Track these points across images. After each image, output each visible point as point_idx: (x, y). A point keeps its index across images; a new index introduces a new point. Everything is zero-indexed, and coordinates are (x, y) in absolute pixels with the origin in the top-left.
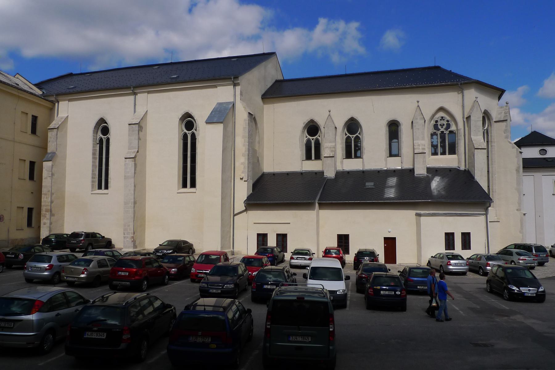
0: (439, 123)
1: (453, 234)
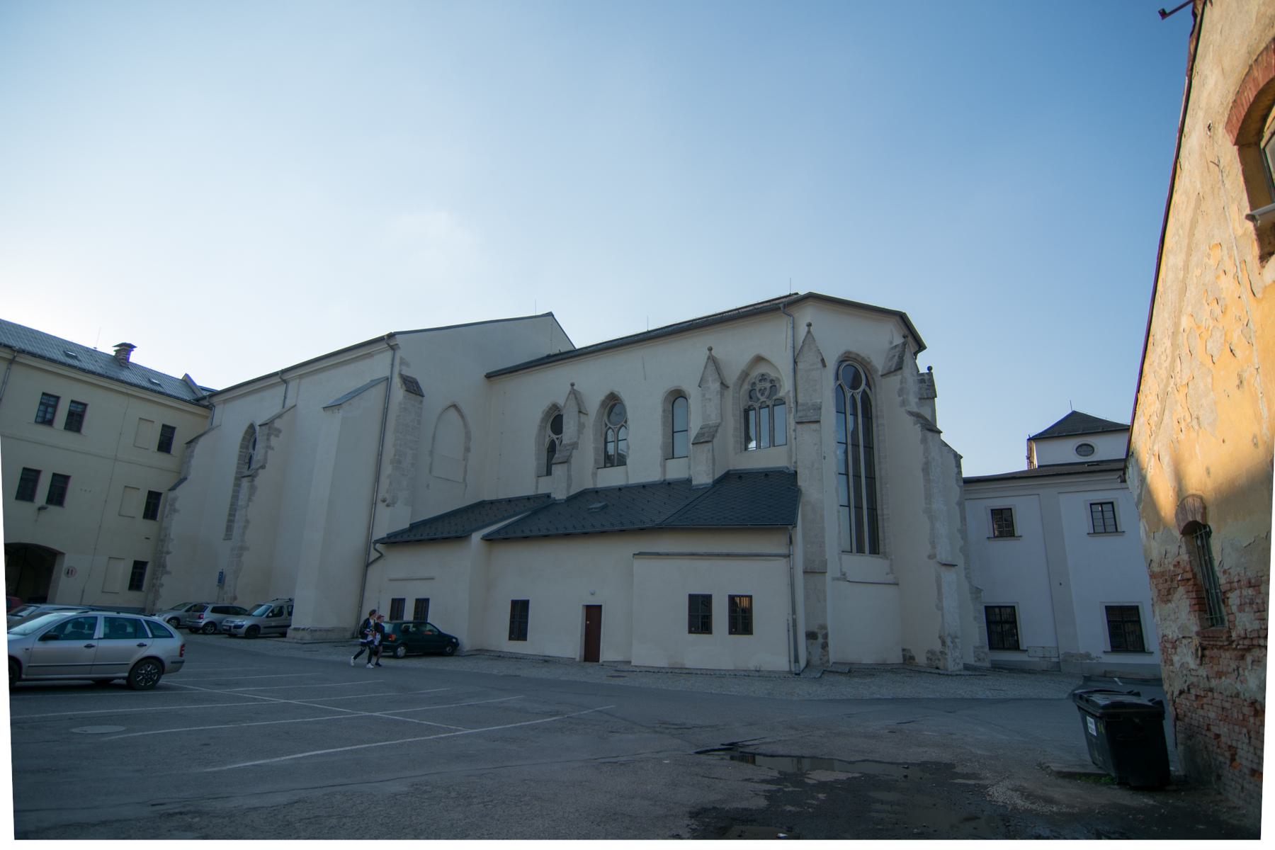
0: (758, 387)
1: (38, 472)
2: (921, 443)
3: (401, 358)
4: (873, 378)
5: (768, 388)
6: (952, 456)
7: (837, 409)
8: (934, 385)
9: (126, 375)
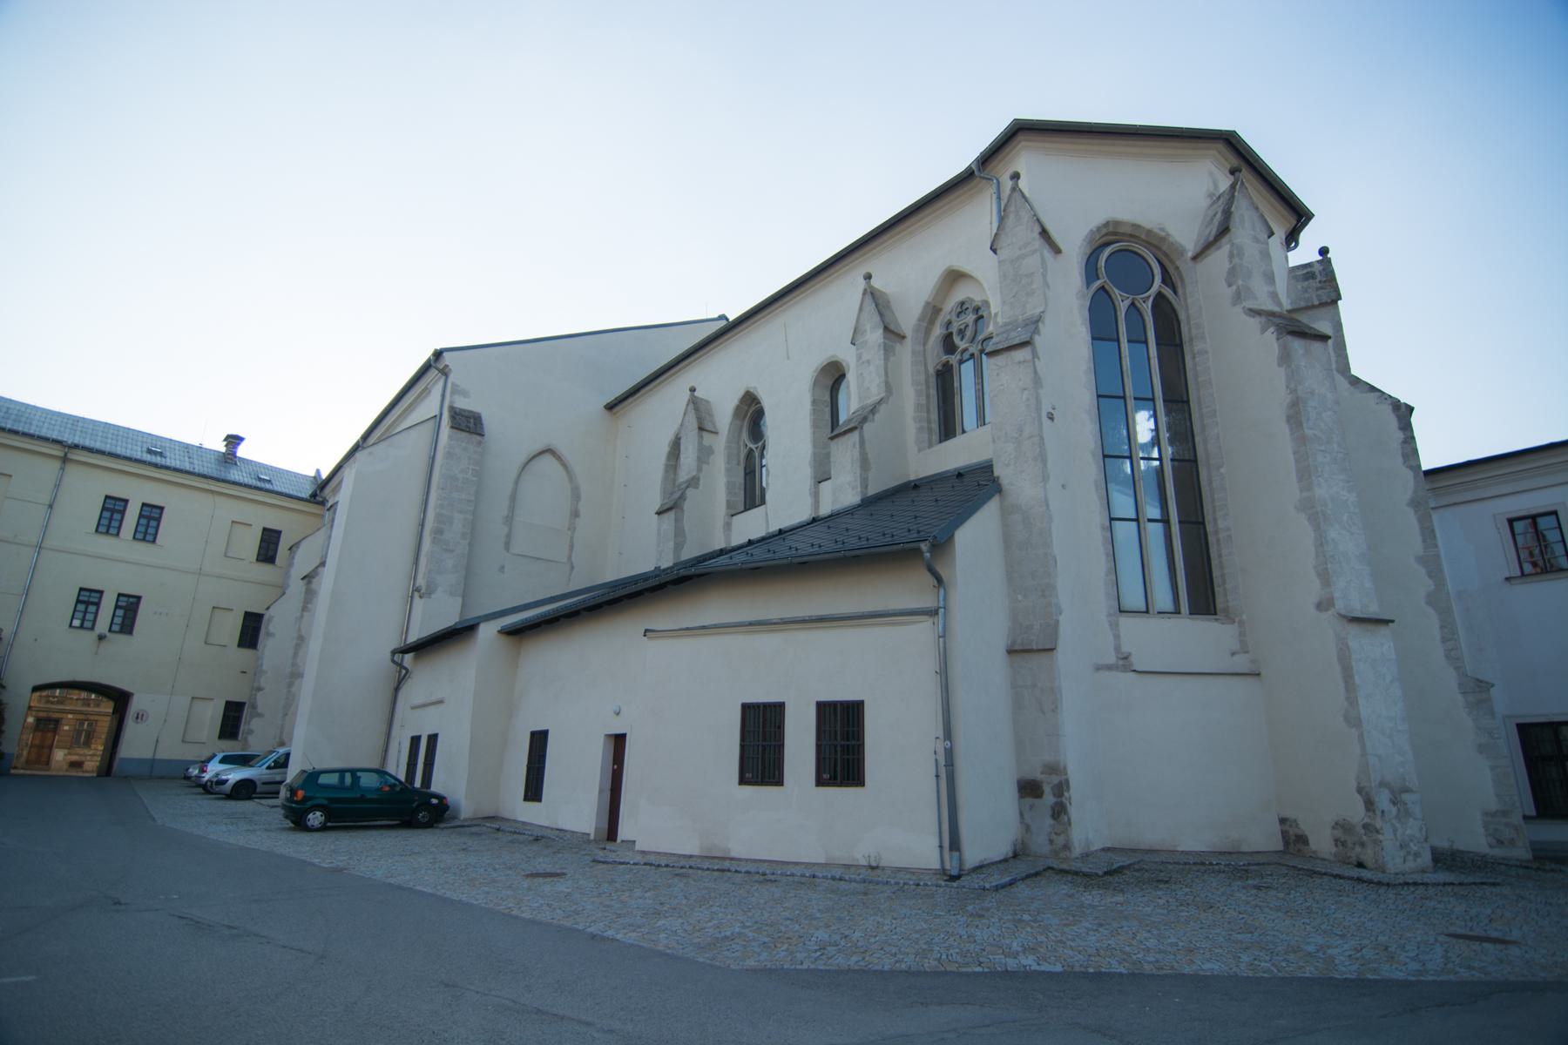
2: (1279, 365)
3: (453, 384)
4: (1177, 268)
5: (971, 324)
6: (1387, 409)
7: (1092, 333)
8: (1334, 279)
9: (235, 475)
